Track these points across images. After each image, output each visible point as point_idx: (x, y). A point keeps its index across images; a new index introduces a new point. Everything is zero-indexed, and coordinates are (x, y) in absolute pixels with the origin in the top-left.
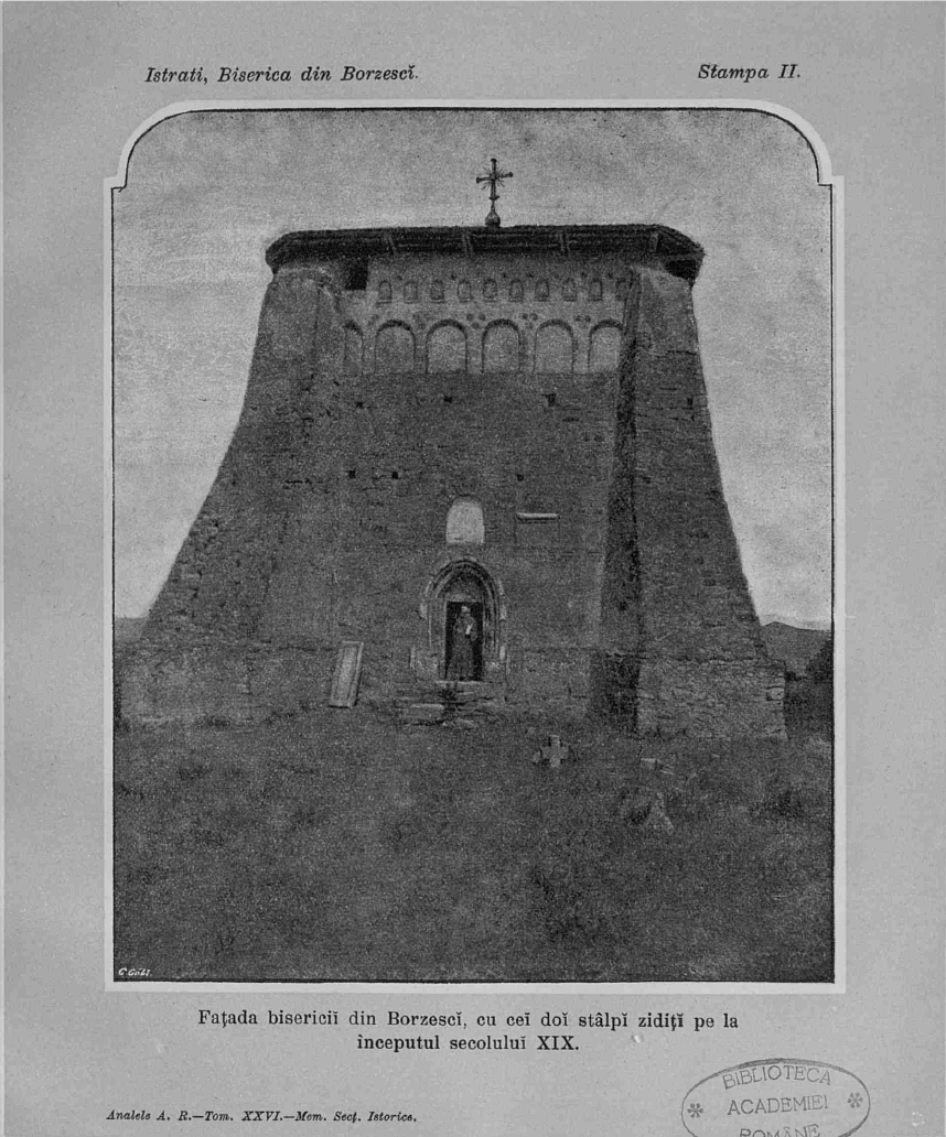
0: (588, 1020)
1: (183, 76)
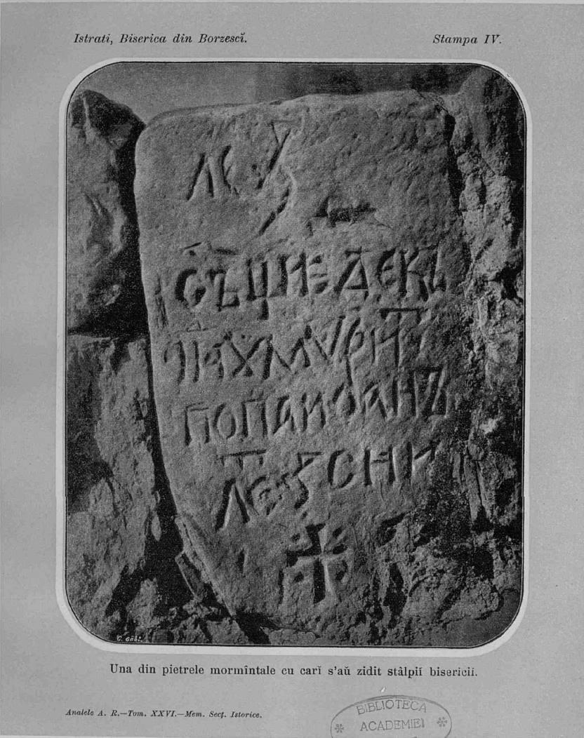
0: (393, 672)
1: (98, 40)
